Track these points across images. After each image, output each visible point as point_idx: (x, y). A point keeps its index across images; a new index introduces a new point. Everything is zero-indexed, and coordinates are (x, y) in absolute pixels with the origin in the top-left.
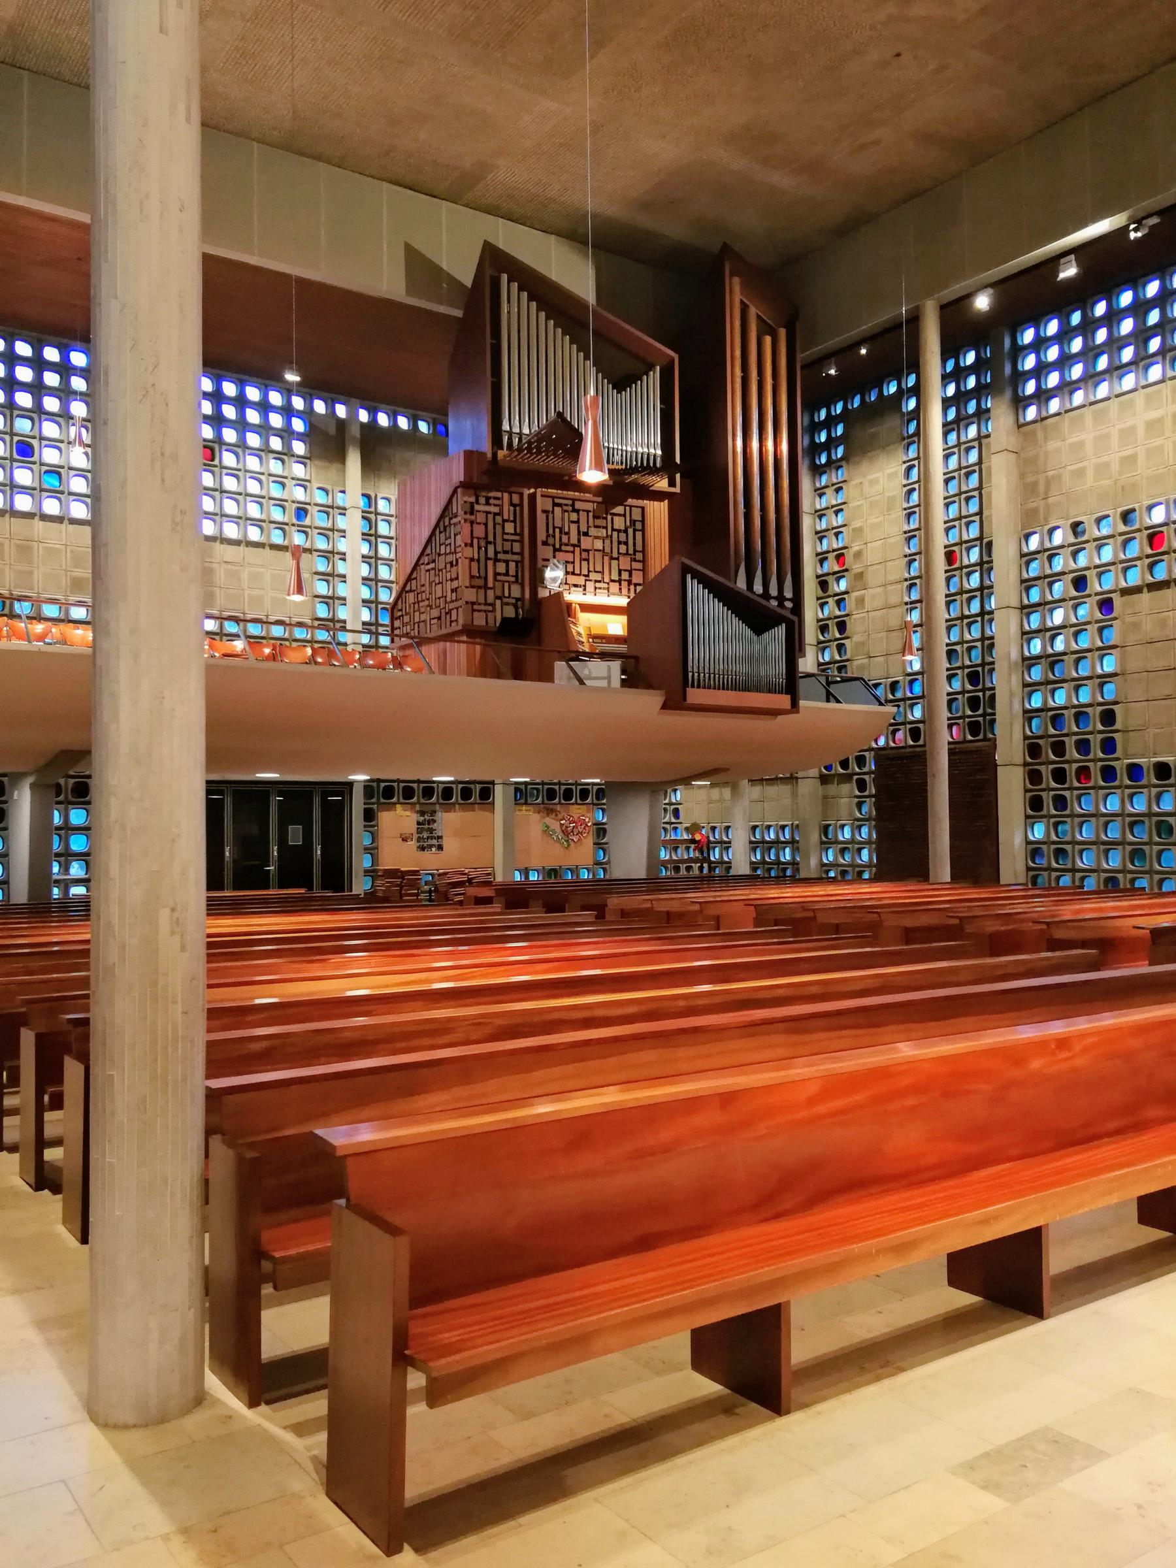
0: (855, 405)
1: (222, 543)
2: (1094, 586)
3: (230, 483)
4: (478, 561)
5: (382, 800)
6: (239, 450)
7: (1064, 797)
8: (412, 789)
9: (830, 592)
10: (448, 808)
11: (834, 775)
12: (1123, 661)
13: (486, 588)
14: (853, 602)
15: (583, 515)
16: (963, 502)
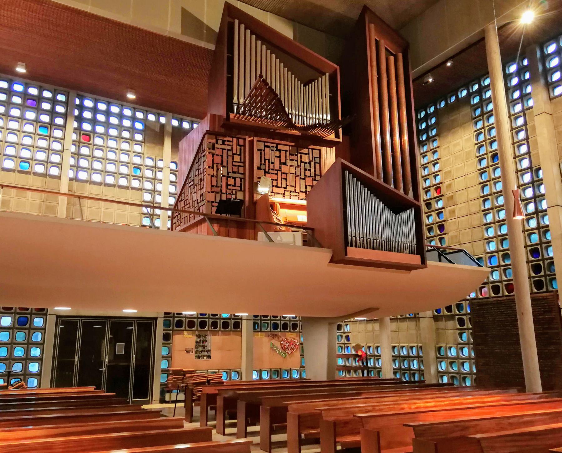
0: (442, 106)
1: (90, 184)
3: (98, 153)
5: (175, 328)
6: (104, 137)
8: (194, 322)
9: (433, 209)
10: (215, 333)
11: (441, 316)
14: (448, 214)
15: (283, 153)
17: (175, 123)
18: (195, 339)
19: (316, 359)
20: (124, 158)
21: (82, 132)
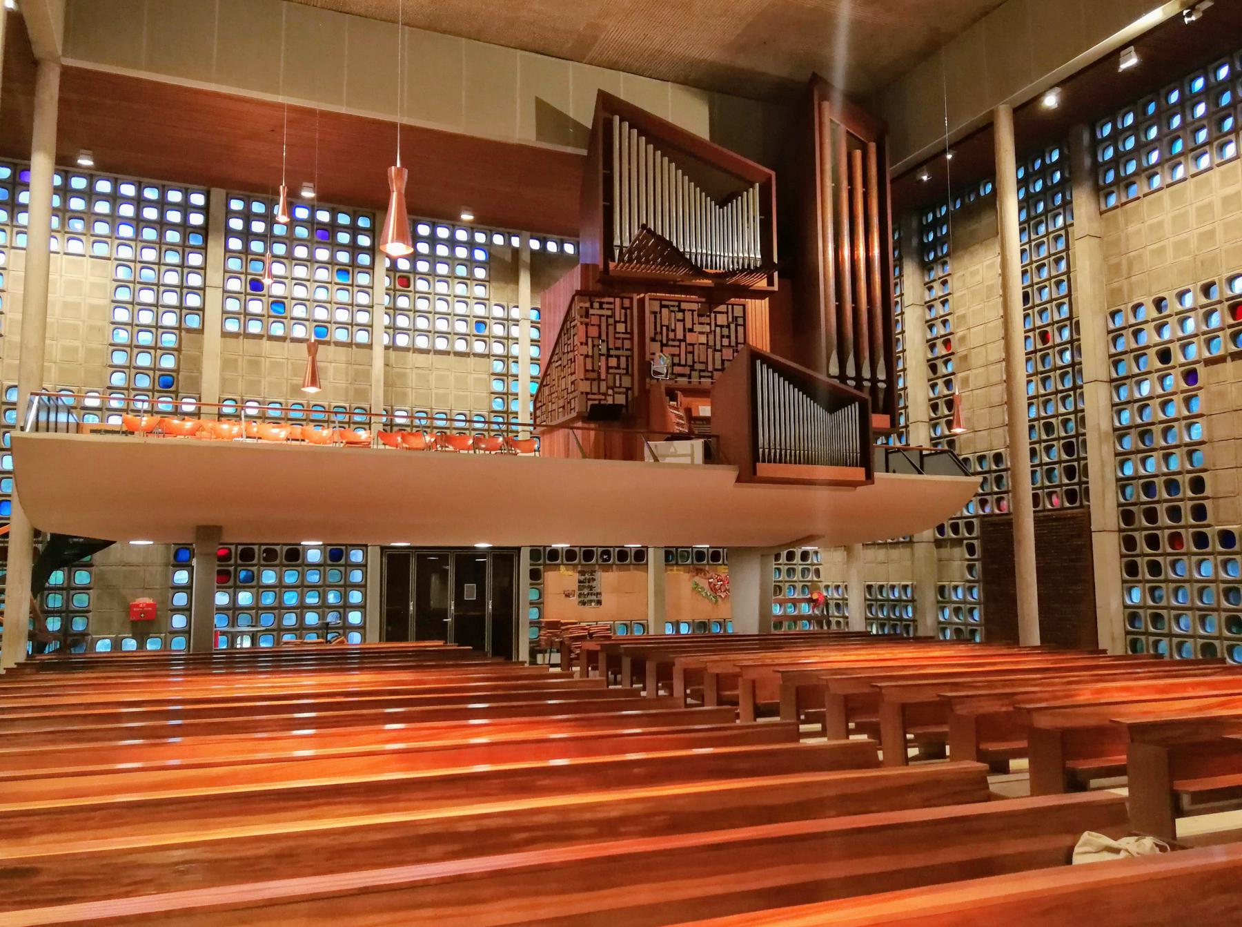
2: (1178, 357)
4: (592, 357)
6: (430, 278)
7: (1158, 563)
8: (574, 552)
9: (939, 374)
10: (607, 568)
12: (1209, 428)
13: (599, 379)
15: (688, 315)
16: (1053, 286)
17: (535, 245)
18: (576, 576)
19: (744, 605)
20: (460, 308)
21: (398, 274)
